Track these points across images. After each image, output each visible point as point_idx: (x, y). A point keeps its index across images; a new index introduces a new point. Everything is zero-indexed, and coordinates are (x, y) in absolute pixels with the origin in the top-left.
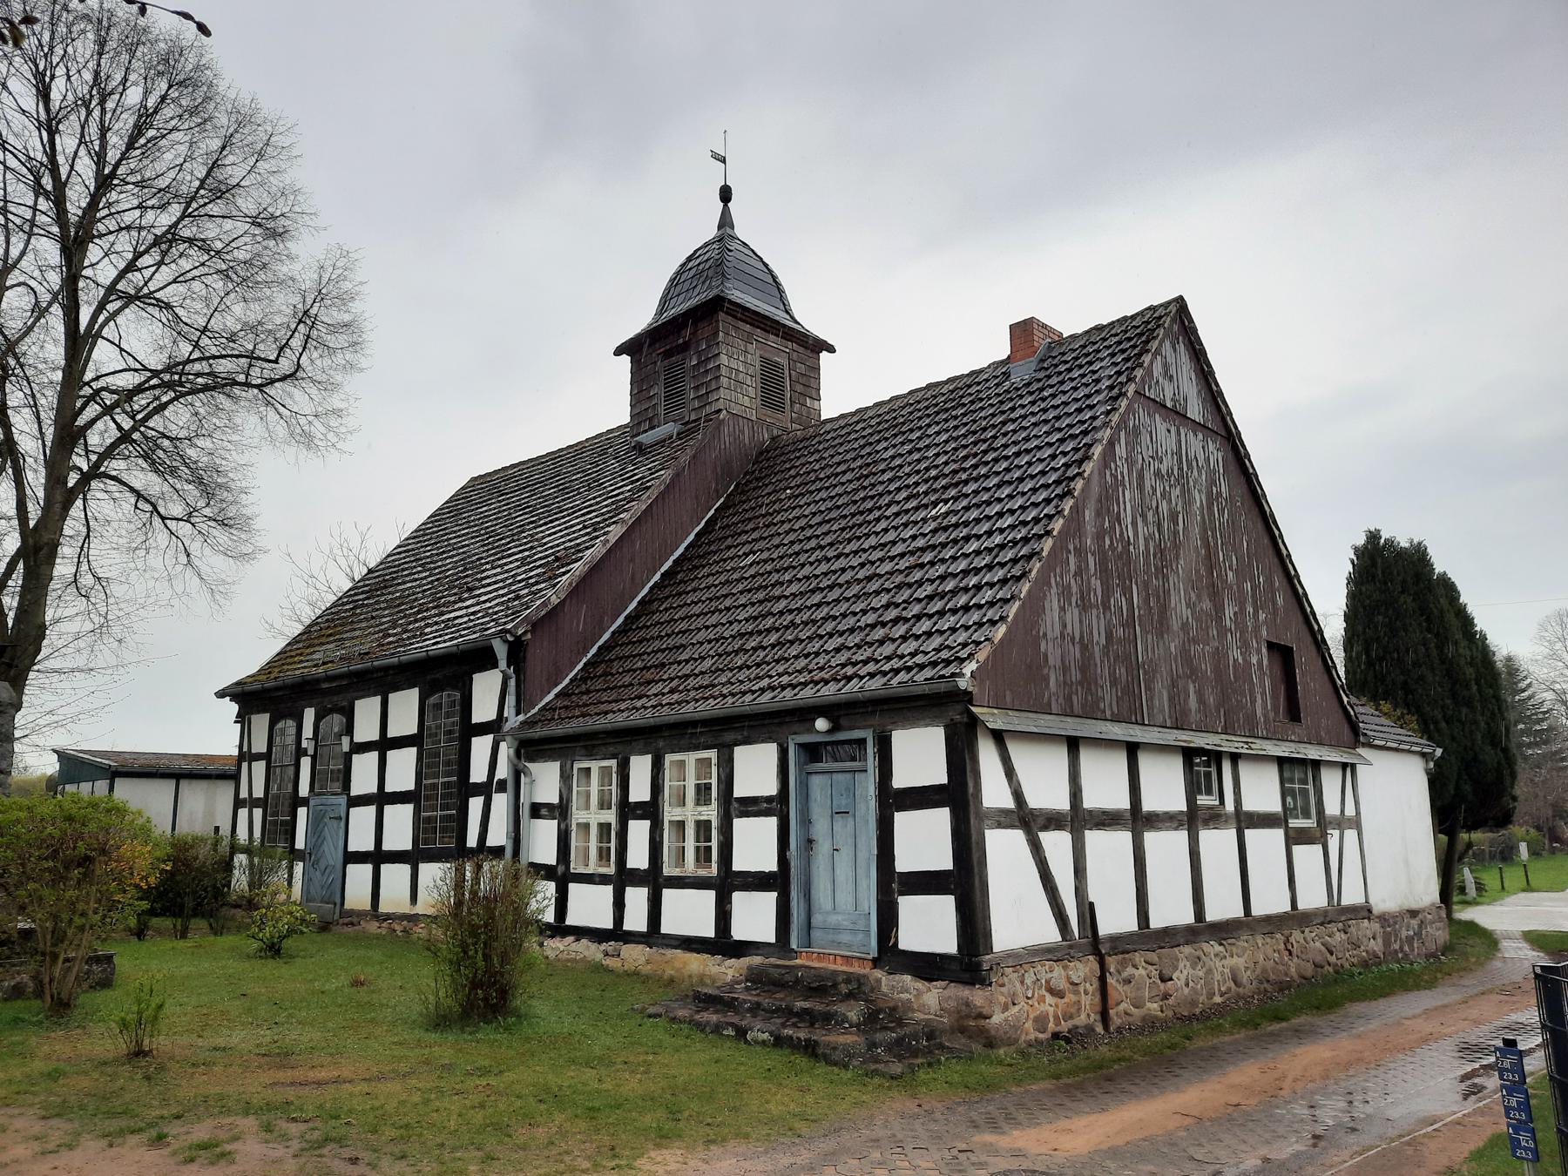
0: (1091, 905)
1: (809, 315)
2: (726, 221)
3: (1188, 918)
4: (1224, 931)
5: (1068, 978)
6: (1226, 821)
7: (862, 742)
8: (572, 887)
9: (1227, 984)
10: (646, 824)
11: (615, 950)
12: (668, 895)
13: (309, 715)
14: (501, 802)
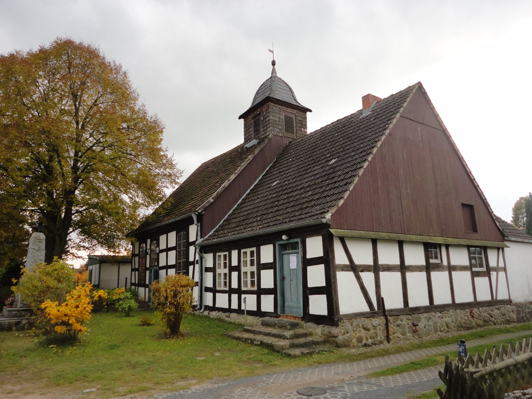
0: (382, 298)
1: (302, 100)
2: (274, 71)
3: (427, 303)
4: (443, 308)
5: (372, 324)
6: (443, 268)
7: (297, 243)
8: (217, 294)
9: (444, 328)
10: (237, 273)
11: (229, 315)
12: (218, 295)
13: (149, 241)
14: (197, 266)
